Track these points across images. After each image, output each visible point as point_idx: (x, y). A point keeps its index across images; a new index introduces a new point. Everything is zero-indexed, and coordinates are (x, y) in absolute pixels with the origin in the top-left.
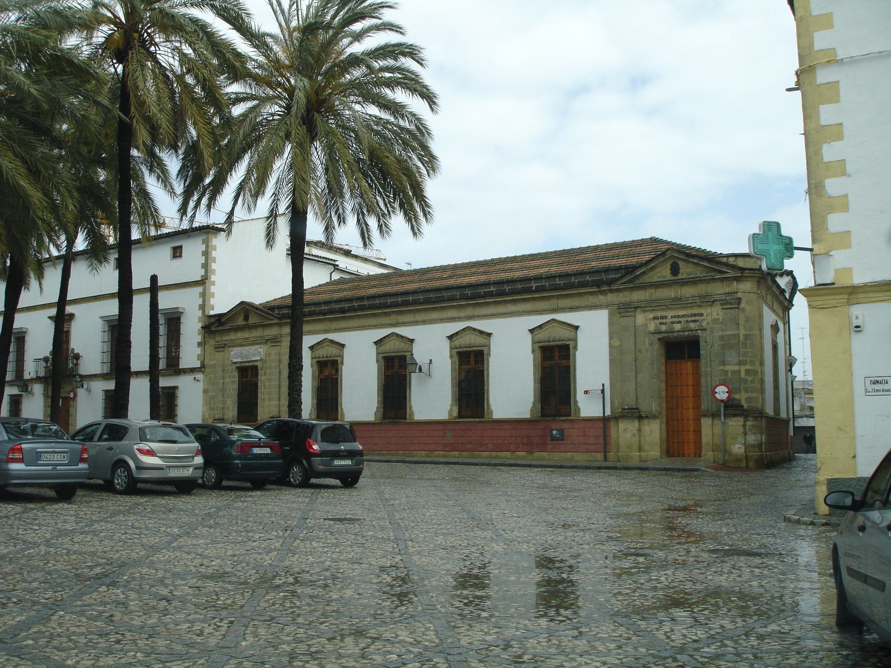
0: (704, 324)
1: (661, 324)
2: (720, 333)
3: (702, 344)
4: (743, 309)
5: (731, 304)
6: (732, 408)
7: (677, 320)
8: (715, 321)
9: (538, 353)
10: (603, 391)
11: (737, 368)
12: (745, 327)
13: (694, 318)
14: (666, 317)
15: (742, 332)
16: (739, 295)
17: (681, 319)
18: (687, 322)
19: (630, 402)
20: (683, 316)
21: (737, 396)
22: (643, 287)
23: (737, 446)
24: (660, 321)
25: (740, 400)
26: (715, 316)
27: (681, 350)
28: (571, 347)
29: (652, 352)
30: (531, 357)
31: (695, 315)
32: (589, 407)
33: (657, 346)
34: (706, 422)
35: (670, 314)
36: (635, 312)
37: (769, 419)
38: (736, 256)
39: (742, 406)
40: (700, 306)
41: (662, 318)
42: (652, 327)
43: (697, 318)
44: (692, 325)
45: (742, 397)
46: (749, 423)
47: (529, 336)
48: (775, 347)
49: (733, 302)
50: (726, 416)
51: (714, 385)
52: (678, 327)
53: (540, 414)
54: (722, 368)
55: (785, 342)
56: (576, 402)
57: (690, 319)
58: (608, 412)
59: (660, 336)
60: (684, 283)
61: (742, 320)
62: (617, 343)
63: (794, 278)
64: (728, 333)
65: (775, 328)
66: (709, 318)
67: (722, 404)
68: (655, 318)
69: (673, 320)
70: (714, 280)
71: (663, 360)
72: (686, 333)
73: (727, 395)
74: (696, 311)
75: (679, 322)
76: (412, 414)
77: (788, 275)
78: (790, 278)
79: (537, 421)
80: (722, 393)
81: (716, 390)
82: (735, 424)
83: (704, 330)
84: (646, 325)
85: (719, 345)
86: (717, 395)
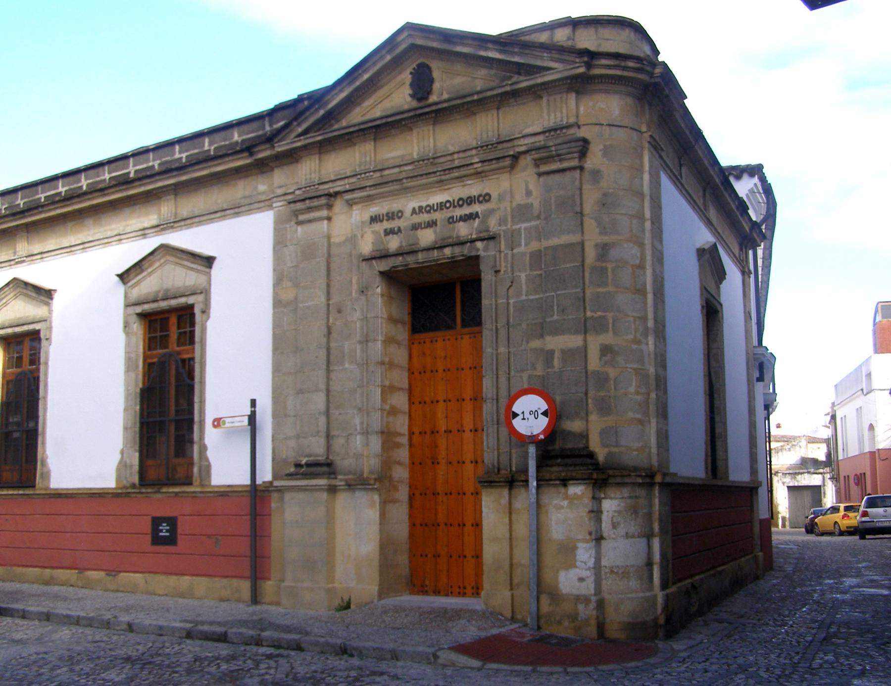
0: (493, 225)
1: (388, 232)
2: (535, 245)
3: (487, 278)
4: (596, 174)
5: (559, 157)
6: (562, 458)
7: (426, 217)
8: (522, 212)
9: (138, 328)
10: (252, 418)
11: (574, 341)
12: (599, 223)
13: (466, 210)
14: (399, 215)
15: (592, 237)
16: (583, 133)
17: (437, 216)
18: (451, 220)
19: (317, 448)
20: (442, 206)
21: (574, 426)
22: (349, 138)
23: (574, 574)
24: (386, 225)
25: (585, 436)
26: (520, 198)
27: (437, 296)
28: (197, 311)
29: (373, 311)
30: (120, 339)
31: (470, 201)
32: (227, 464)
33: (378, 289)
34: (492, 508)
35: (409, 204)
36: (330, 207)
37: (680, 493)
38: (575, 24)
39: (591, 455)
40: (478, 174)
41: (391, 216)
42: (367, 247)
43: (476, 208)
44: (464, 230)
45: (595, 432)
46: (610, 506)
47: (121, 289)
48: (712, 312)
49: (564, 152)
50: (541, 481)
51: (514, 391)
52: (427, 237)
53: (136, 479)
54: (535, 344)
55: (748, 315)
56: (203, 449)
57: (458, 212)
58: (265, 475)
59: (384, 266)
60: (440, 115)
61: (591, 199)
62: (288, 295)
63: (763, 179)
64: (555, 241)
65: (709, 260)
66: (506, 206)
67: (532, 450)
68: (374, 219)
69: (417, 219)
70: (515, 95)
71: (402, 333)
72: (447, 251)
73: (544, 421)
74: (474, 188)
75: (432, 224)
76: (46, 476)
77: (752, 175)
78: (756, 180)
79: (128, 494)
80: (530, 416)
81: (516, 408)
82: (566, 510)
83: (492, 238)
84: (352, 240)
85: (529, 279)
86: (517, 423)
